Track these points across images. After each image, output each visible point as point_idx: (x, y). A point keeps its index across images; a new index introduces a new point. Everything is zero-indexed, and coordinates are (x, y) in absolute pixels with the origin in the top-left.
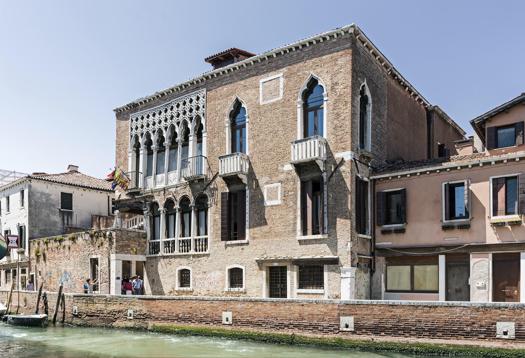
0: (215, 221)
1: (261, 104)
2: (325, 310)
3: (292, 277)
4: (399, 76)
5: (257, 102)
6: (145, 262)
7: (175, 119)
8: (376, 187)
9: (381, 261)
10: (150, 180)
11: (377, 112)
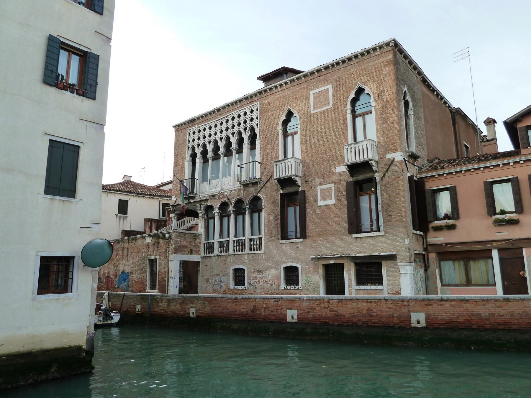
0: (269, 221)
1: (312, 112)
3: (350, 275)
5: (308, 111)
7: (230, 130)
10: (206, 185)
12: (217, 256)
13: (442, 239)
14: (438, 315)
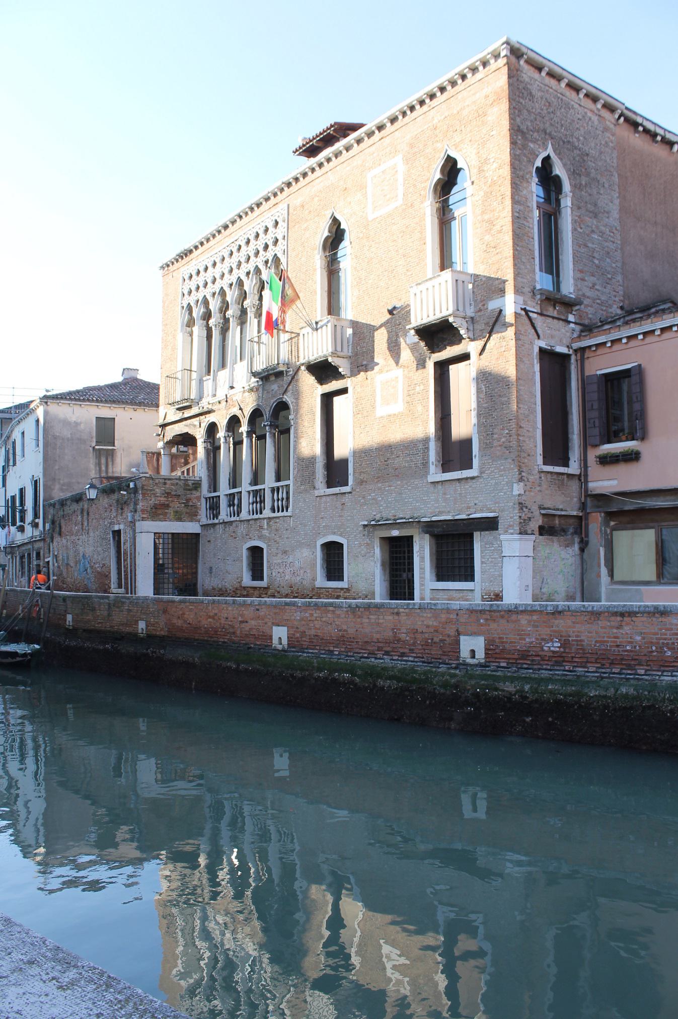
1: (371, 217)
2: (435, 624)
3: (422, 559)
4: (646, 123)
6: (198, 535)
8: (587, 363)
9: (596, 523)
11: (589, 209)
12: (224, 523)
13: (615, 483)
14: (506, 642)
